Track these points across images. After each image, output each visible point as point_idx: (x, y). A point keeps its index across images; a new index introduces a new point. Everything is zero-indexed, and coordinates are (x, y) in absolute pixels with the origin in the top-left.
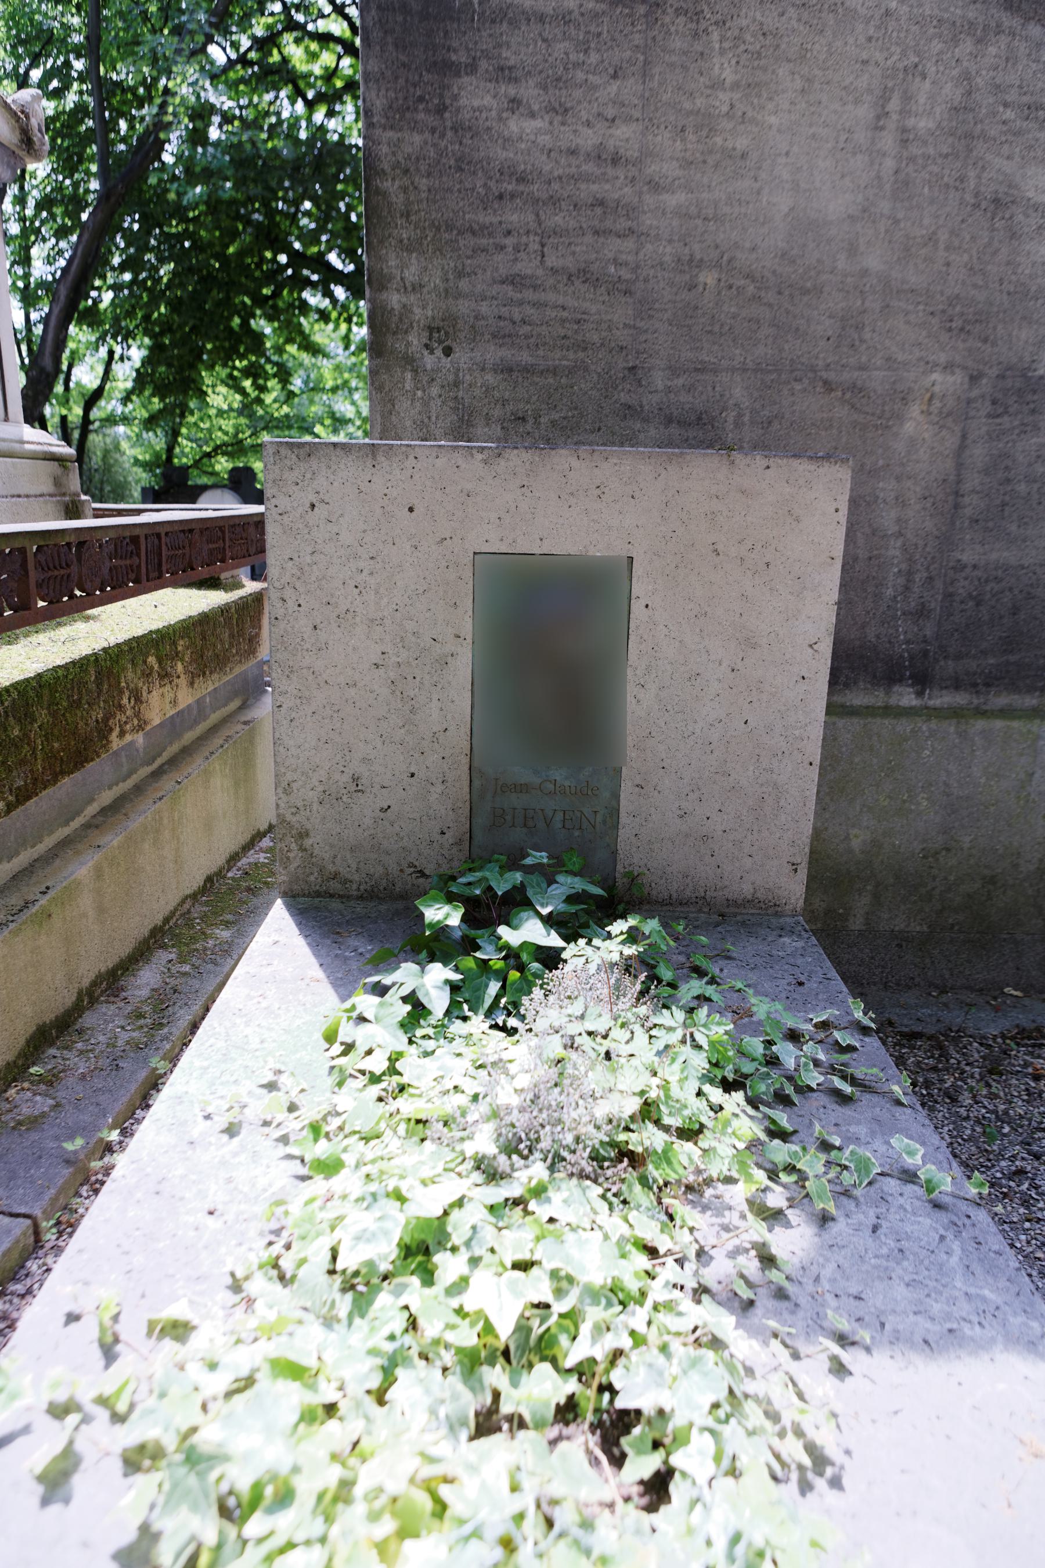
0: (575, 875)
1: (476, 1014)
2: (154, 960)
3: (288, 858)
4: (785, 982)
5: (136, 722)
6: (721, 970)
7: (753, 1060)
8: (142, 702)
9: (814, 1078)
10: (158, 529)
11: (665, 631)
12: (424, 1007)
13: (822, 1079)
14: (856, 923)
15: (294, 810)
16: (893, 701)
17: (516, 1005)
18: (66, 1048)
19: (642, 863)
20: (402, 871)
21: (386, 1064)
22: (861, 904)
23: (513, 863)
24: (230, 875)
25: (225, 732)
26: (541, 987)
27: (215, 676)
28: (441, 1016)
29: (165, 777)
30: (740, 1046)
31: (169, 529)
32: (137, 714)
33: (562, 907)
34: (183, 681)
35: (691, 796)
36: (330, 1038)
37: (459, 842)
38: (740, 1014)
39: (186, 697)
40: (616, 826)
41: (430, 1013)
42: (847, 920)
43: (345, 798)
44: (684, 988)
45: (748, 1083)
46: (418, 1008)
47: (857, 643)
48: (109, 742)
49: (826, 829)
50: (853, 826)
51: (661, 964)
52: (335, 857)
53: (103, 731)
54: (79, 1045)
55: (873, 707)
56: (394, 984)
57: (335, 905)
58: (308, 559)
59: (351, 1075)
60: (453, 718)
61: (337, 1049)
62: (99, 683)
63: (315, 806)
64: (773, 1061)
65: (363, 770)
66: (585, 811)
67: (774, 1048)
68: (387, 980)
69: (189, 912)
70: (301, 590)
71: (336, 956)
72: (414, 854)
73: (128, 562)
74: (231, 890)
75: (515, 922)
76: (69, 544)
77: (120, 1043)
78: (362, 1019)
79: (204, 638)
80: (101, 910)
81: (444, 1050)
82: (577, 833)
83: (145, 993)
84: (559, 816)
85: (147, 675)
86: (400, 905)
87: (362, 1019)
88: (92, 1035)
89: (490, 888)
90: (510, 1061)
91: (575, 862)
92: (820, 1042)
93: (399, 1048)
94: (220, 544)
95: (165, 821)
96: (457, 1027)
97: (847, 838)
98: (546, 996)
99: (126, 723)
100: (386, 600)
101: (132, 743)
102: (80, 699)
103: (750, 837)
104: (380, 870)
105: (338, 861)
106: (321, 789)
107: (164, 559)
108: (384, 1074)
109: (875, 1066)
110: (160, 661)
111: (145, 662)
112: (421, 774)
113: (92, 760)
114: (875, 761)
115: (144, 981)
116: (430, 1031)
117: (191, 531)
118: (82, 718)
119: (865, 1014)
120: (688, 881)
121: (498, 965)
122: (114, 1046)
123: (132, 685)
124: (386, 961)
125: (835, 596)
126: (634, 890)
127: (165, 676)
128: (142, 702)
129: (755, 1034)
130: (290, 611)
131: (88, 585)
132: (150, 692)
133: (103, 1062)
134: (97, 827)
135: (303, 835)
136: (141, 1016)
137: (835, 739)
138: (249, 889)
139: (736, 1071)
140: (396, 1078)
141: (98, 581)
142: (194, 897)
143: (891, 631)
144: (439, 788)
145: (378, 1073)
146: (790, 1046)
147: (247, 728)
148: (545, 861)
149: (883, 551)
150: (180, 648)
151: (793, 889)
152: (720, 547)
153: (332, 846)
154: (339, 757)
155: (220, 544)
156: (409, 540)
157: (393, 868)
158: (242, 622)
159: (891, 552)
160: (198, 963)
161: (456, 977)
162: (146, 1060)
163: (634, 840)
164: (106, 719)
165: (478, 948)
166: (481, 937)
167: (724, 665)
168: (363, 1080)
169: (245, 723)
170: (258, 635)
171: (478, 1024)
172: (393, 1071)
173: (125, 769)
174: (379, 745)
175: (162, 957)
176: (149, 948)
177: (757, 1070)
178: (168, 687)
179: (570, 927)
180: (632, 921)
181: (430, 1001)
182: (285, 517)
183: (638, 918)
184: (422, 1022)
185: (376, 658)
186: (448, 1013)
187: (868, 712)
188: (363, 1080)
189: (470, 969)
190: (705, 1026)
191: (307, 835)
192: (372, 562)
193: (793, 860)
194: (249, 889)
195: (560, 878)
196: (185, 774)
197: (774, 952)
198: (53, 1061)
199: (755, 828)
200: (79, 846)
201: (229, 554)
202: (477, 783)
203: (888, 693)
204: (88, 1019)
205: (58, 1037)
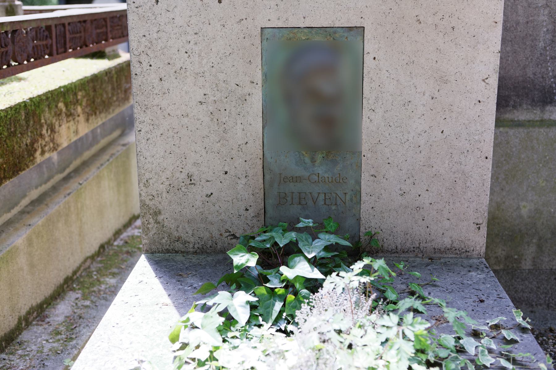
0: (331, 233)
1: (267, 323)
2: (67, 298)
3: (148, 228)
4: (472, 300)
5: (51, 145)
6: (429, 294)
7: (448, 349)
8: (55, 132)
9: (488, 360)
10: (63, 21)
11: (387, 74)
12: (233, 318)
13: (493, 361)
14: (527, 265)
15: (151, 197)
16: (546, 116)
17: (293, 316)
18: (12, 354)
19: (377, 226)
20: (221, 235)
21: (208, 354)
22: (530, 252)
23: (292, 228)
24: (116, 243)
25: (110, 151)
26: (308, 304)
27: (103, 115)
28: (244, 324)
29: (72, 181)
30: (439, 340)
31: (70, 20)
32: (52, 140)
33: (323, 254)
34: (82, 118)
35: (408, 181)
36: (174, 340)
37: (257, 216)
38: (440, 321)
39: (84, 129)
40: (359, 202)
41: (237, 322)
42: (520, 263)
43: (183, 189)
44: (401, 303)
45: (444, 363)
46: (229, 320)
47: (521, 79)
48: (34, 158)
49: (504, 203)
50: (522, 200)
51: (389, 290)
52: (178, 227)
53: (31, 151)
54: (20, 352)
55: (533, 121)
56: (214, 304)
57: (179, 257)
58: (155, 36)
59: (186, 362)
60: (251, 135)
61: (178, 345)
62: (27, 121)
63: (164, 195)
64: (461, 350)
65: (194, 170)
66: (339, 193)
67: (461, 341)
68: (210, 303)
69: (89, 267)
70: (152, 56)
71: (179, 289)
72: (229, 224)
73: (44, 43)
74: (116, 254)
75: (291, 264)
76: (6, 32)
77: (46, 350)
78: (194, 327)
79: (95, 91)
80: (32, 266)
81: (243, 344)
82: (334, 207)
83: (61, 319)
84: (322, 197)
85: (58, 114)
86: (220, 257)
87: (194, 327)
88: (28, 346)
89: (276, 244)
90: (287, 351)
91: (332, 226)
92: (494, 337)
93: (217, 344)
94: (104, 30)
95: (72, 209)
96: (255, 331)
97: (518, 208)
98: (311, 309)
99: (45, 146)
100: (205, 61)
101: (50, 159)
102: (15, 131)
103: (448, 207)
104: (207, 235)
105: (180, 229)
106: (168, 183)
107: (68, 40)
108: (207, 360)
109: (529, 352)
110: (66, 105)
111: (57, 106)
112: (231, 172)
113: (24, 169)
114: (535, 156)
115: (61, 311)
116: (237, 334)
117: (85, 21)
118: (17, 142)
119: (524, 319)
120: (408, 237)
121: (281, 291)
122: (42, 352)
123: (48, 122)
124: (211, 291)
125: (499, 48)
126: (373, 244)
127: (70, 115)
128: (55, 132)
129: (451, 332)
130: (145, 70)
131: (19, 58)
132: (60, 126)
133: (35, 362)
134: (28, 213)
135: (157, 213)
136: (58, 333)
137: (508, 143)
138: (128, 252)
139: (436, 357)
140: (214, 363)
141: (25, 55)
142: (92, 258)
143: (543, 70)
144: (244, 181)
145: (203, 360)
146: (472, 340)
147: (124, 148)
148: (311, 225)
149: (536, 17)
150: (79, 97)
151: (478, 241)
152: (421, 18)
153: (176, 220)
154: (178, 162)
155: (104, 30)
156: (219, 21)
157: (216, 234)
158: (118, 81)
159: (542, 18)
160: (95, 299)
161: (254, 299)
162: (62, 361)
163: (371, 211)
164: (32, 144)
165: (268, 281)
166: (270, 274)
167: (427, 95)
168: (194, 364)
169: (124, 145)
170: (130, 88)
171: (267, 329)
172: (212, 358)
173: (46, 176)
174: (204, 154)
175: (72, 296)
176: (63, 291)
177: (449, 355)
178: (72, 123)
179: (326, 265)
180: (367, 261)
181: (237, 315)
182: (140, 9)
183: (370, 259)
184: (232, 328)
185: (200, 98)
186: (248, 322)
187: (530, 124)
188: (194, 364)
189: (263, 294)
190: (412, 325)
191: (160, 213)
192: (196, 36)
193: (477, 221)
194: (128, 252)
195: (321, 236)
196: (85, 178)
197: (465, 282)
198: (3, 362)
199: (451, 201)
200: (17, 225)
201: (110, 35)
202: (267, 177)
203: (542, 111)
204: (25, 336)
205: (6, 347)
